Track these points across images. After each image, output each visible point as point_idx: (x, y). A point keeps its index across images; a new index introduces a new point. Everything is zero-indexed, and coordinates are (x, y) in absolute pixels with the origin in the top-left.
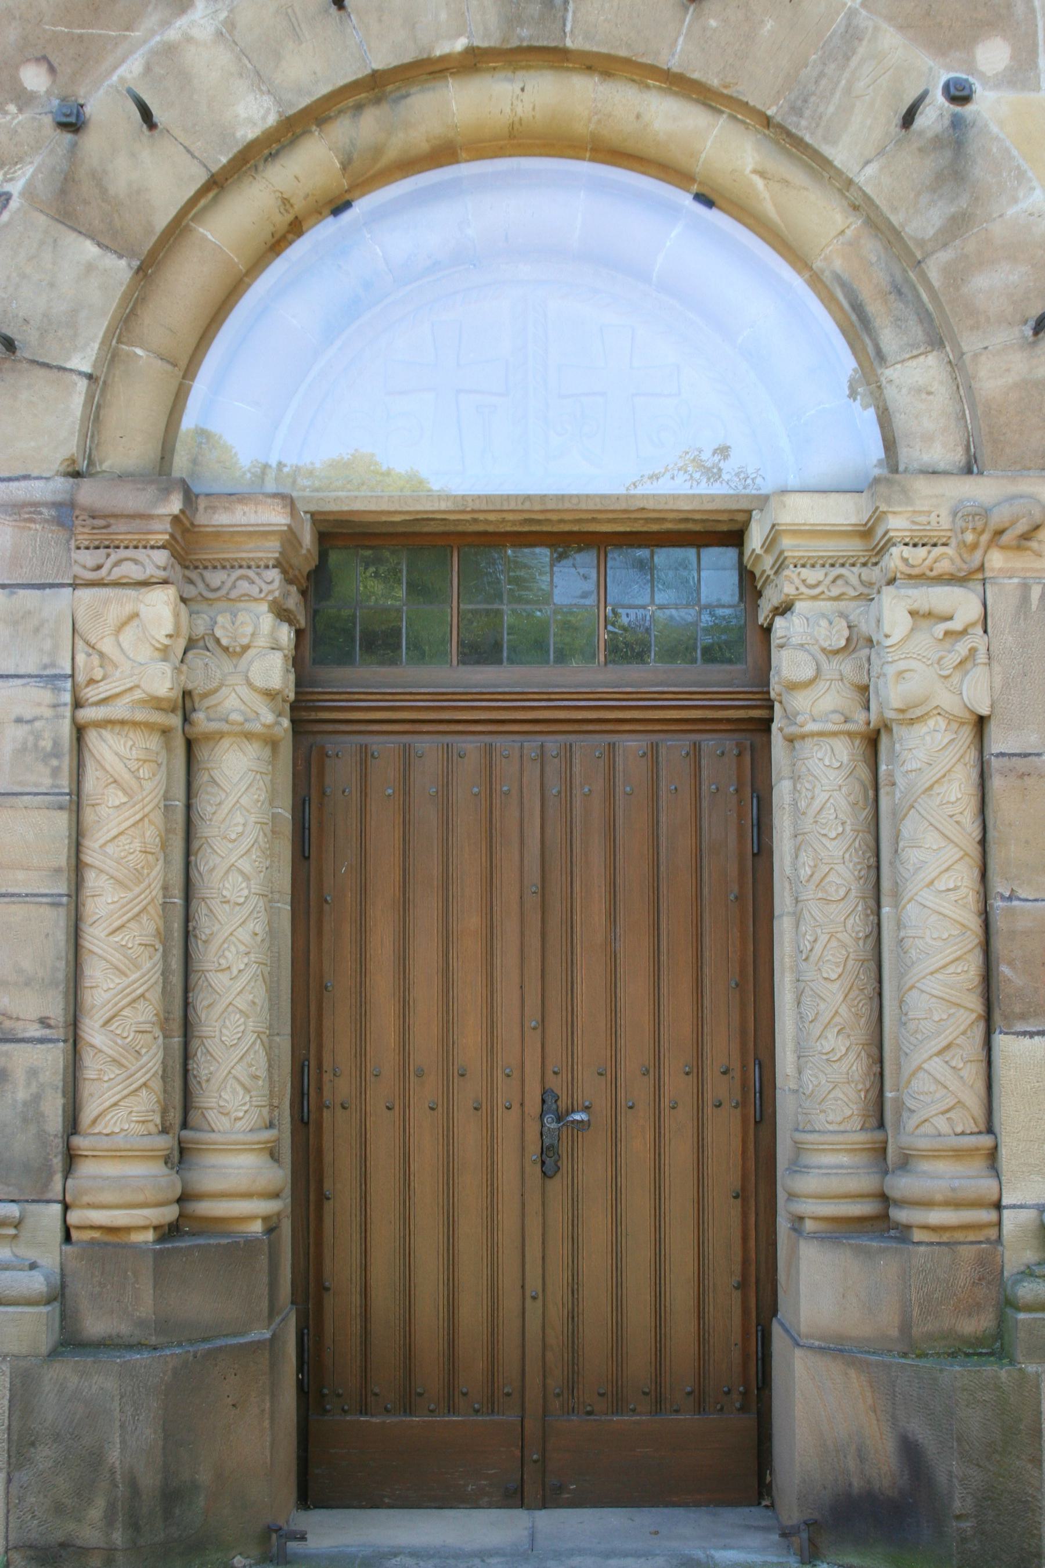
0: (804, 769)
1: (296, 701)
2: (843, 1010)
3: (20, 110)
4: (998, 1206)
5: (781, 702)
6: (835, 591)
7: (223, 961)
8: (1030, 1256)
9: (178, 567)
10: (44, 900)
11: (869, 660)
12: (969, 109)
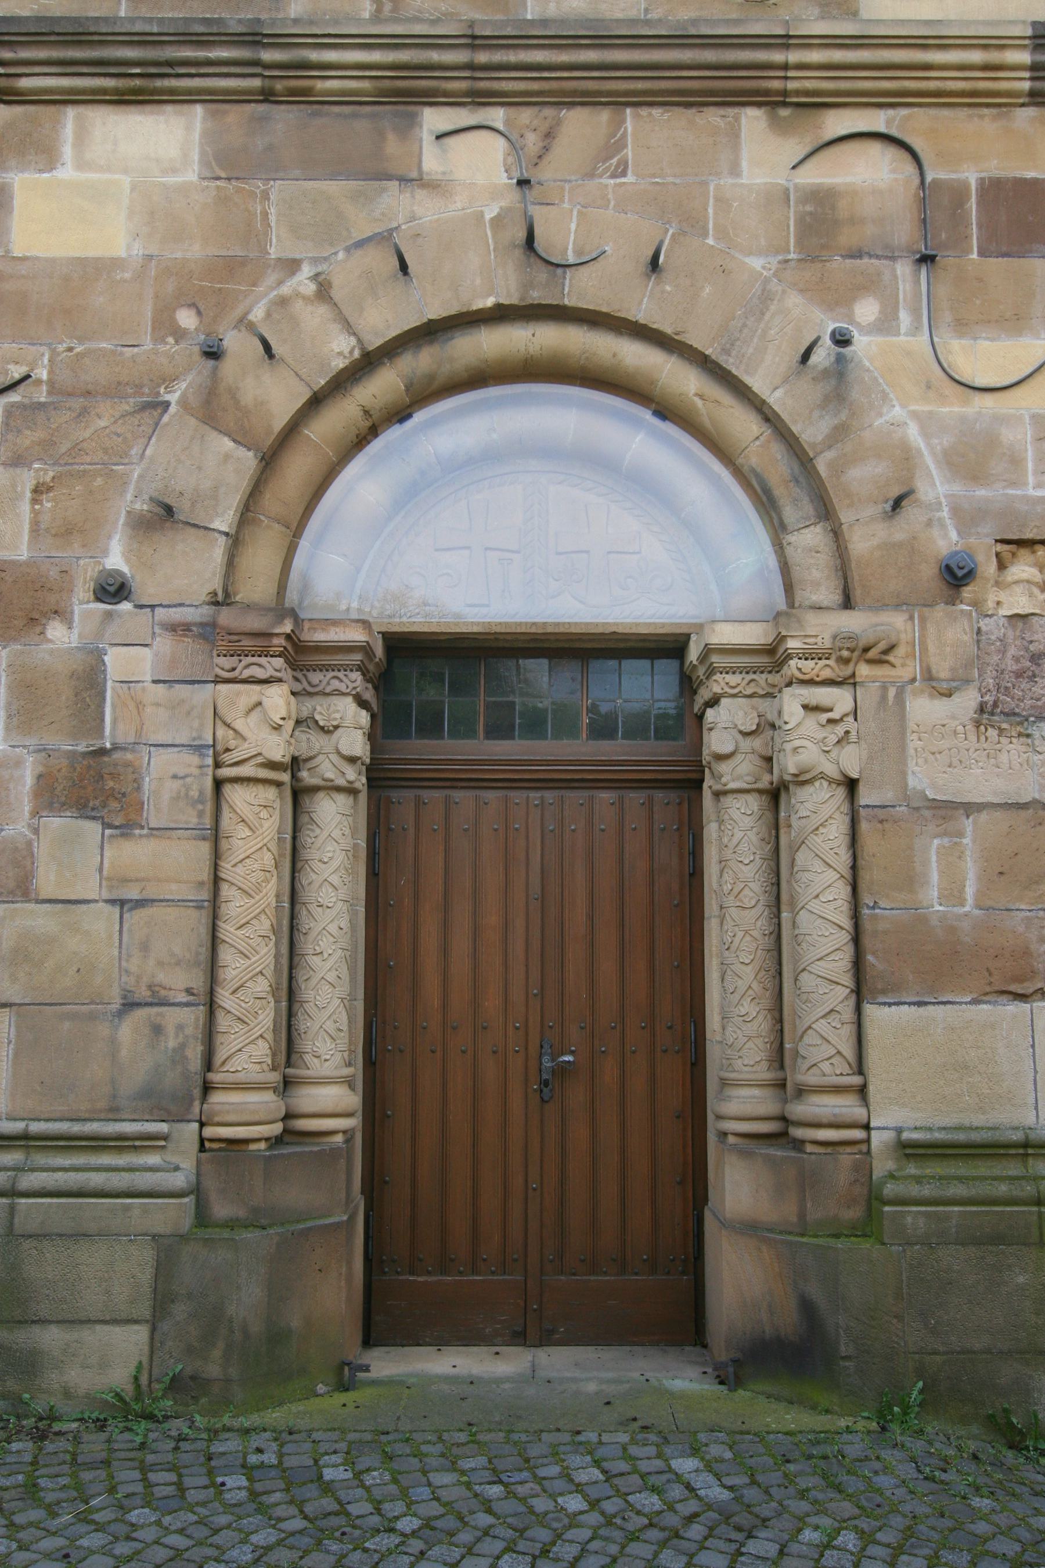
0: (726, 817)
1: (371, 764)
2: (755, 985)
3: (177, 342)
4: (867, 1127)
5: (710, 768)
6: (749, 692)
7: (317, 948)
8: (890, 1165)
9: (289, 670)
10: (191, 904)
11: (772, 738)
12: (847, 351)
